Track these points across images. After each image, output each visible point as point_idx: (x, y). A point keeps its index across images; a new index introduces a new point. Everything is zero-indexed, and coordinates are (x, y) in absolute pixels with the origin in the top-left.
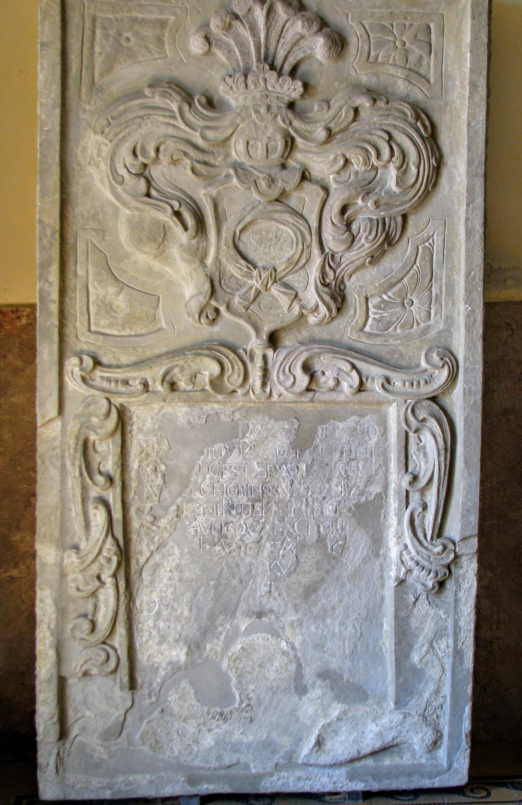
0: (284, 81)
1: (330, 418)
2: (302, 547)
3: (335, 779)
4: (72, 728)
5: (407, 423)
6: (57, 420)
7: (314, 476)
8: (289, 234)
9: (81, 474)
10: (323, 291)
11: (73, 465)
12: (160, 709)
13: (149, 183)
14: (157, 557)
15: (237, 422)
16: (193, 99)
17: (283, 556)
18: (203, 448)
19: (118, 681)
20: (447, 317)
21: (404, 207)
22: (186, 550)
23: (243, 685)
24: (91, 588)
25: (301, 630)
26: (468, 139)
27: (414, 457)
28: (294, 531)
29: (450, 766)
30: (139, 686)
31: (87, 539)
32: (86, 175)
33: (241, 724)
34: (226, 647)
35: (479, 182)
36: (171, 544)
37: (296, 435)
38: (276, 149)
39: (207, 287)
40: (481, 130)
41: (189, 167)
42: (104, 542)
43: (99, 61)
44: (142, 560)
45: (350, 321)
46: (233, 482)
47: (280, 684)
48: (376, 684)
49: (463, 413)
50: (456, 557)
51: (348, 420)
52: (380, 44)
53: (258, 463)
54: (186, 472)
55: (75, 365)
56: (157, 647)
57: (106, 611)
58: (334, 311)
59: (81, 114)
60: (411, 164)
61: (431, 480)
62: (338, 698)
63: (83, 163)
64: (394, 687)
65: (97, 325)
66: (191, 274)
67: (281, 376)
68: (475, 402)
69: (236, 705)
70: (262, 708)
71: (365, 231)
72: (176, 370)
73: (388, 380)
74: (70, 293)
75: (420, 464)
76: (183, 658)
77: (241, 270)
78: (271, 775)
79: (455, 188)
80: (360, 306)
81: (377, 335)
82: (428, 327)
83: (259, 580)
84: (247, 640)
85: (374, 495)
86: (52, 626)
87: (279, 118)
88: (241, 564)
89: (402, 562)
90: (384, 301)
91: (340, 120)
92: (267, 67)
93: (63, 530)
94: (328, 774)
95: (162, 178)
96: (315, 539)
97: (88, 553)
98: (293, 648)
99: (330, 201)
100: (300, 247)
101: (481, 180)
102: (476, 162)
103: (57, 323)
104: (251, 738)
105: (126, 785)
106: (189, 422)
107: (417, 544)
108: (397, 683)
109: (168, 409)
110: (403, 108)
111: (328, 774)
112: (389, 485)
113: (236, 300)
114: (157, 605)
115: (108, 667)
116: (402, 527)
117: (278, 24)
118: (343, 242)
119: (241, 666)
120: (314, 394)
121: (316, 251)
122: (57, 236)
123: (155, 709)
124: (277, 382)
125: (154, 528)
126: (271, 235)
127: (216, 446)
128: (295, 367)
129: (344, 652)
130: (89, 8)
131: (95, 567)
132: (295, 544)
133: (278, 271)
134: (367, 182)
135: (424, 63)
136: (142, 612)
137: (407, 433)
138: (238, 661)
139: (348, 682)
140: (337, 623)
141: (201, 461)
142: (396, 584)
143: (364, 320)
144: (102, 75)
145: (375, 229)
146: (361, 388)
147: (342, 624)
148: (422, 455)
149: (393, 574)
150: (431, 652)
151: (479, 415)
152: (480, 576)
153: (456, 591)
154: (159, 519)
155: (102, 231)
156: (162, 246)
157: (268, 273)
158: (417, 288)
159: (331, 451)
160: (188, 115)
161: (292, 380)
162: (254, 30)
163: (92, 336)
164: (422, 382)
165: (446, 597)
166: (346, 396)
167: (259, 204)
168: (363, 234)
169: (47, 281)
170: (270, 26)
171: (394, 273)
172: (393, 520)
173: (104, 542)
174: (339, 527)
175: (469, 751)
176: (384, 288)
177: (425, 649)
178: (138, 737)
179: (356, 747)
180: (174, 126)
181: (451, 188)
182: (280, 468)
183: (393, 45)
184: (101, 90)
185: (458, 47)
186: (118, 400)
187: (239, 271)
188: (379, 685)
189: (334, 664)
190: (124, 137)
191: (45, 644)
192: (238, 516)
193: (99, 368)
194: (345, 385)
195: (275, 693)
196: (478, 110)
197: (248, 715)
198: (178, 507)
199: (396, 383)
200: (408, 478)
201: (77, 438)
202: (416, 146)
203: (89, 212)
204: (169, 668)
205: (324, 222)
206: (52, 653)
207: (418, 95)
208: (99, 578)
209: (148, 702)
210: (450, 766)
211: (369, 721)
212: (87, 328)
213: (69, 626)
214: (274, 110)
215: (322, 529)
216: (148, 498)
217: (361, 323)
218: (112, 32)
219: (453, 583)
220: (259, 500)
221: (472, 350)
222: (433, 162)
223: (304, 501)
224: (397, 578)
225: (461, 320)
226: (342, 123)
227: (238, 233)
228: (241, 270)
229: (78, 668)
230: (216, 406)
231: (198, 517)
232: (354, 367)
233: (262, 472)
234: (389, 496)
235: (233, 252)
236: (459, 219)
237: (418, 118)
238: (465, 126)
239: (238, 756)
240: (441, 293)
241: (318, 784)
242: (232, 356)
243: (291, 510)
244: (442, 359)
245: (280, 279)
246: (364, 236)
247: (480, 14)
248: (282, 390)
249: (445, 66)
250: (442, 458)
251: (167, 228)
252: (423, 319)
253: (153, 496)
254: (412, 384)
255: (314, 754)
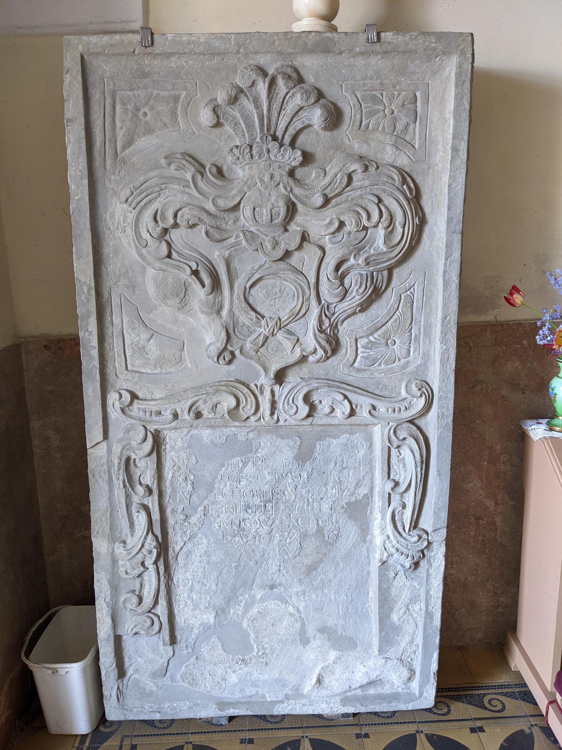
0: (285, 150)
1: (326, 436)
2: (304, 536)
3: (332, 705)
4: (128, 669)
5: (389, 441)
6: (103, 443)
7: (314, 482)
8: (291, 288)
9: (125, 486)
10: (320, 337)
11: (118, 479)
12: (195, 657)
13: (169, 245)
14: (189, 546)
15: (251, 440)
16: (205, 168)
17: (289, 544)
18: (224, 461)
19: (161, 637)
20: (424, 354)
21: (390, 262)
22: (212, 540)
23: (259, 639)
24: (137, 572)
25: (304, 598)
26: (449, 200)
27: (395, 467)
28: (298, 524)
29: (421, 695)
30: (179, 640)
31: (132, 535)
32: (115, 237)
33: (258, 667)
34: (246, 611)
35: (457, 238)
36: (200, 535)
37: (299, 449)
38: (279, 214)
39: (223, 335)
40: (460, 191)
41: (203, 231)
42: (145, 538)
43: (120, 134)
44: (177, 548)
45: (342, 359)
46: (249, 487)
47: (288, 638)
48: (364, 636)
49: (436, 432)
50: (429, 543)
51: (341, 438)
52: (371, 114)
53: (268, 472)
54: (211, 480)
55: (115, 399)
56: (191, 613)
57: (150, 588)
58: (329, 354)
59: (107, 184)
60: (397, 223)
61: (409, 486)
62: (334, 647)
63: (112, 228)
64: (378, 639)
65: (132, 365)
66: (209, 323)
67: (286, 406)
68: (447, 424)
69: (254, 654)
70: (275, 655)
71: (356, 285)
72: (200, 403)
73: (374, 408)
74: (108, 340)
75: (400, 473)
76: (212, 620)
77: (252, 320)
78: (282, 702)
79: (435, 243)
80: (351, 346)
81: (365, 370)
82: (408, 362)
83: (270, 561)
84: (262, 606)
85: (362, 495)
86: (108, 600)
87: (281, 185)
88: (256, 550)
89: (385, 548)
90: (370, 341)
91: (336, 186)
92: (270, 138)
93: (113, 527)
94: (326, 701)
95: (181, 241)
96: (315, 530)
97: (133, 547)
98: (298, 611)
99: (326, 260)
100: (301, 299)
101: (459, 236)
102: (455, 221)
103: (97, 365)
104: (266, 677)
105: (171, 710)
106: (212, 442)
107: (398, 535)
108: (380, 637)
109: (195, 432)
110: (391, 172)
111: (326, 701)
112: (374, 488)
113: (248, 345)
114: (190, 581)
115: (153, 630)
116: (385, 521)
117: (279, 96)
118: (337, 296)
119: (258, 625)
120: (314, 419)
121: (314, 302)
122: (93, 292)
123: (192, 657)
124: (282, 411)
125: (186, 524)
126: (277, 290)
127: (234, 460)
128: (297, 399)
129: (339, 614)
130: (108, 86)
131: (140, 557)
132: (299, 534)
133: (282, 321)
134: (358, 241)
135: (410, 129)
136: (178, 587)
137: (389, 448)
138: (255, 622)
139: (341, 635)
140: (333, 592)
141: (222, 471)
142: (380, 564)
143: (354, 358)
144: (124, 148)
145: (364, 282)
146: (352, 413)
147: (337, 593)
148: (401, 465)
149: (377, 556)
150: (407, 613)
151: (450, 434)
152: (447, 557)
153: (428, 569)
154: (190, 517)
155: (132, 287)
156: (184, 300)
157: (274, 321)
158: (399, 330)
159: (327, 462)
160: (201, 184)
161: (295, 409)
162: (258, 106)
163: (129, 374)
164: (403, 409)
165: (420, 573)
166: (339, 420)
167: (265, 263)
168: (354, 288)
169: (87, 331)
170: (272, 98)
171: (379, 318)
172: (377, 515)
173: (145, 538)
174: (334, 521)
175: (436, 684)
176: (371, 331)
177: (402, 611)
178: (179, 676)
179: (348, 683)
180: (189, 194)
181: (431, 243)
182: (286, 476)
183: (383, 113)
184: (124, 161)
185: (442, 113)
186: (152, 428)
187: (250, 321)
188: (366, 637)
189: (330, 622)
190: (145, 205)
191: (102, 613)
192: (253, 514)
193: (136, 401)
194: (338, 412)
195: (284, 644)
196: (458, 172)
197: (264, 660)
198: (205, 508)
199: (381, 410)
200: (391, 485)
201: (120, 458)
202: (402, 208)
203: (120, 271)
204: (201, 628)
205: (321, 278)
206: (109, 620)
207: (403, 161)
208: (143, 564)
209: (185, 652)
210: (421, 695)
211: (358, 663)
212: (124, 368)
213: (122, 599)
214: (277, 178)
215: (320, 522)
216: (180, 501)
217: (351, 360)
218: (130, 107)
219: (426, 562)
220: (270, 501)
221: (446, 382)
222: (417, 221)
223: (306, 501)
224: (381, 560)
225: (437, 357)
226: (336, 188)
227: (248, 288)
228: (252, 320)
229: (130, 630)
230: (233, 429)
231: (221, 515)
232: (346, 397)
233: (272, 479)
234: (374, 496)
235: (244, 304)
236: (438, 270)
237: (404, 182)
238: (447, 187)
239: (257, 689)
240: (420, 334)
241: (319, 709)
242: (246, 390)
243: (295, 508)
244: (420, 389)
245: (284, 327)
246: (355, 289)
247: (463, 83)
248: (287, 417)
249: (429, 132)
250: (419, 469)
251: (187, 285)
252: (404, 356)
253: (185, 500)
254: (394, 411)
255: (316, 690)
